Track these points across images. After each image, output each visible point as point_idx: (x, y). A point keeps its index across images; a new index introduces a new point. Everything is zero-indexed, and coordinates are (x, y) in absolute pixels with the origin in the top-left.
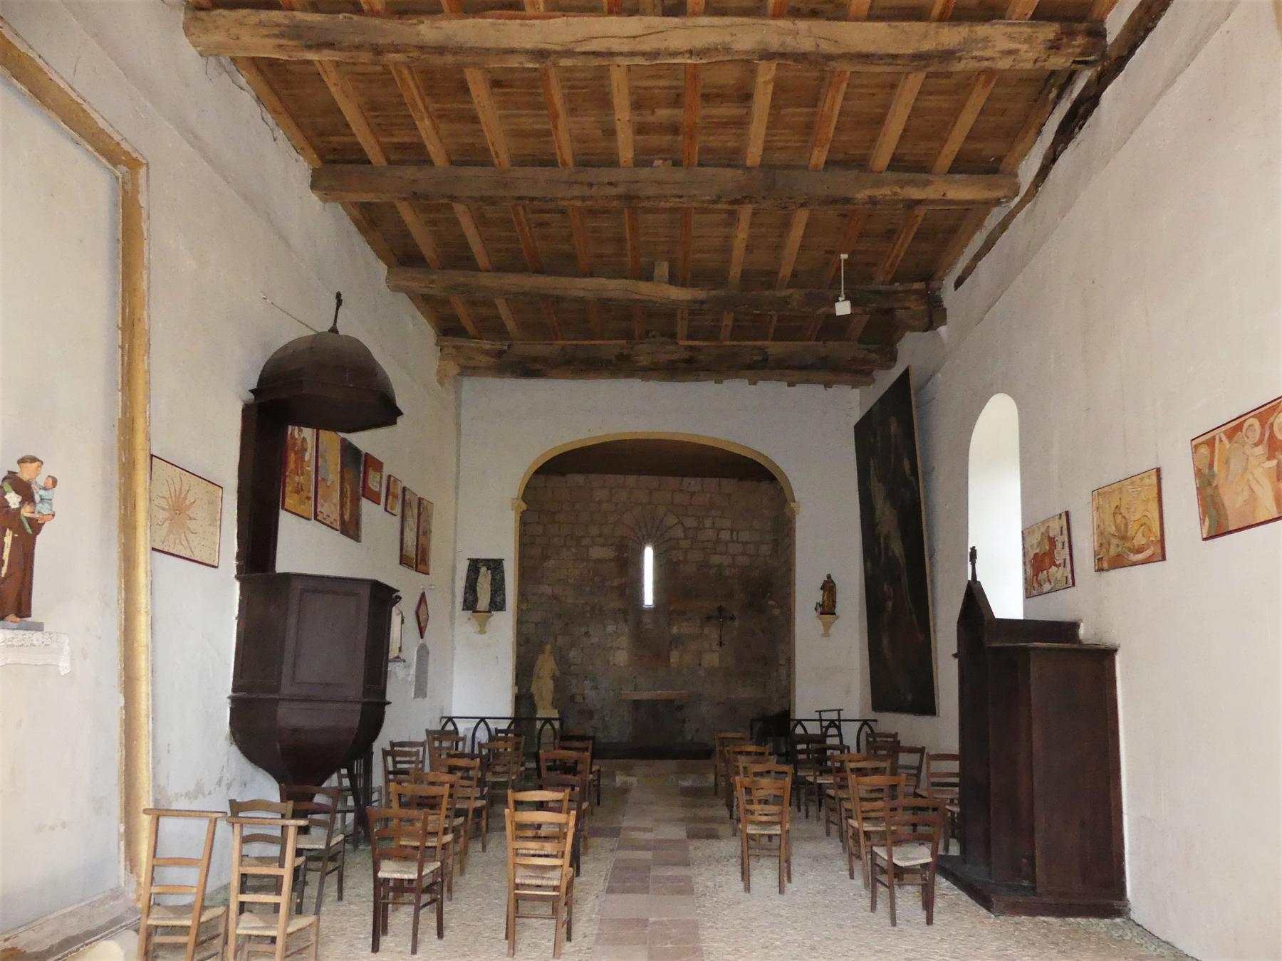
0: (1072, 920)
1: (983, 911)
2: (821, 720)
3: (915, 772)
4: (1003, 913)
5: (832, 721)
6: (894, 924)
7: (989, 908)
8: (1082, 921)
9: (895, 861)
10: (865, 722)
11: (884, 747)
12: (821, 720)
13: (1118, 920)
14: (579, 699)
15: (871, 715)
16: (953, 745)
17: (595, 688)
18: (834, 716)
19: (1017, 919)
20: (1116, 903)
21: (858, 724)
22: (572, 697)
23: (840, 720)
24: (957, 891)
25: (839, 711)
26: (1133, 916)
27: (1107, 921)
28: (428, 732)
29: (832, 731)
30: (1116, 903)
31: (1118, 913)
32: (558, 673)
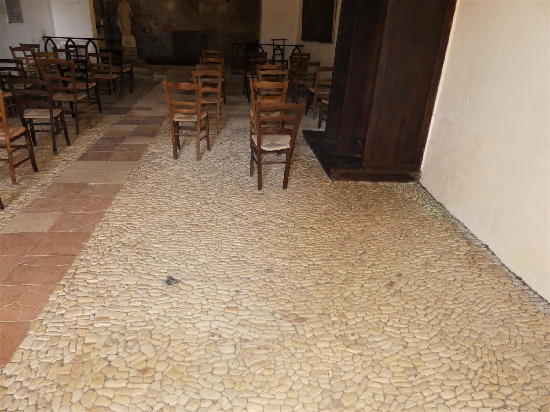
0: (382, 183)
1: (326, 176)
2: (274, 45)
3: (312, 77)
4: (337, 179)
5: (278, 46)
6: (260, 188)
7: (329, 174)
8: (388, 184)
9: (262, 147)
10: (297, 47)
11: (301, 62)
12: (274, 45)
13: (411, 183)
14: (148, 30)
15: (302, 43)
16: (331, 62)
17: (156, 24)
18: (281, 43)
19: (346, 183)
20: (412, 174)
21: (294, 47)
22: (144, 29)
23: (284, 45)
24: (314, 159)
25: (284, 40)
26: (421, 181)
27: (404, 184)
28: (309, 55)
29: (278, 52)
30: (412, 174)
31: (412, 179)
32: (132, 15)
